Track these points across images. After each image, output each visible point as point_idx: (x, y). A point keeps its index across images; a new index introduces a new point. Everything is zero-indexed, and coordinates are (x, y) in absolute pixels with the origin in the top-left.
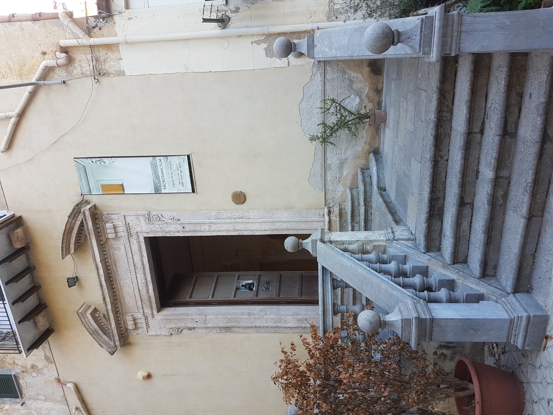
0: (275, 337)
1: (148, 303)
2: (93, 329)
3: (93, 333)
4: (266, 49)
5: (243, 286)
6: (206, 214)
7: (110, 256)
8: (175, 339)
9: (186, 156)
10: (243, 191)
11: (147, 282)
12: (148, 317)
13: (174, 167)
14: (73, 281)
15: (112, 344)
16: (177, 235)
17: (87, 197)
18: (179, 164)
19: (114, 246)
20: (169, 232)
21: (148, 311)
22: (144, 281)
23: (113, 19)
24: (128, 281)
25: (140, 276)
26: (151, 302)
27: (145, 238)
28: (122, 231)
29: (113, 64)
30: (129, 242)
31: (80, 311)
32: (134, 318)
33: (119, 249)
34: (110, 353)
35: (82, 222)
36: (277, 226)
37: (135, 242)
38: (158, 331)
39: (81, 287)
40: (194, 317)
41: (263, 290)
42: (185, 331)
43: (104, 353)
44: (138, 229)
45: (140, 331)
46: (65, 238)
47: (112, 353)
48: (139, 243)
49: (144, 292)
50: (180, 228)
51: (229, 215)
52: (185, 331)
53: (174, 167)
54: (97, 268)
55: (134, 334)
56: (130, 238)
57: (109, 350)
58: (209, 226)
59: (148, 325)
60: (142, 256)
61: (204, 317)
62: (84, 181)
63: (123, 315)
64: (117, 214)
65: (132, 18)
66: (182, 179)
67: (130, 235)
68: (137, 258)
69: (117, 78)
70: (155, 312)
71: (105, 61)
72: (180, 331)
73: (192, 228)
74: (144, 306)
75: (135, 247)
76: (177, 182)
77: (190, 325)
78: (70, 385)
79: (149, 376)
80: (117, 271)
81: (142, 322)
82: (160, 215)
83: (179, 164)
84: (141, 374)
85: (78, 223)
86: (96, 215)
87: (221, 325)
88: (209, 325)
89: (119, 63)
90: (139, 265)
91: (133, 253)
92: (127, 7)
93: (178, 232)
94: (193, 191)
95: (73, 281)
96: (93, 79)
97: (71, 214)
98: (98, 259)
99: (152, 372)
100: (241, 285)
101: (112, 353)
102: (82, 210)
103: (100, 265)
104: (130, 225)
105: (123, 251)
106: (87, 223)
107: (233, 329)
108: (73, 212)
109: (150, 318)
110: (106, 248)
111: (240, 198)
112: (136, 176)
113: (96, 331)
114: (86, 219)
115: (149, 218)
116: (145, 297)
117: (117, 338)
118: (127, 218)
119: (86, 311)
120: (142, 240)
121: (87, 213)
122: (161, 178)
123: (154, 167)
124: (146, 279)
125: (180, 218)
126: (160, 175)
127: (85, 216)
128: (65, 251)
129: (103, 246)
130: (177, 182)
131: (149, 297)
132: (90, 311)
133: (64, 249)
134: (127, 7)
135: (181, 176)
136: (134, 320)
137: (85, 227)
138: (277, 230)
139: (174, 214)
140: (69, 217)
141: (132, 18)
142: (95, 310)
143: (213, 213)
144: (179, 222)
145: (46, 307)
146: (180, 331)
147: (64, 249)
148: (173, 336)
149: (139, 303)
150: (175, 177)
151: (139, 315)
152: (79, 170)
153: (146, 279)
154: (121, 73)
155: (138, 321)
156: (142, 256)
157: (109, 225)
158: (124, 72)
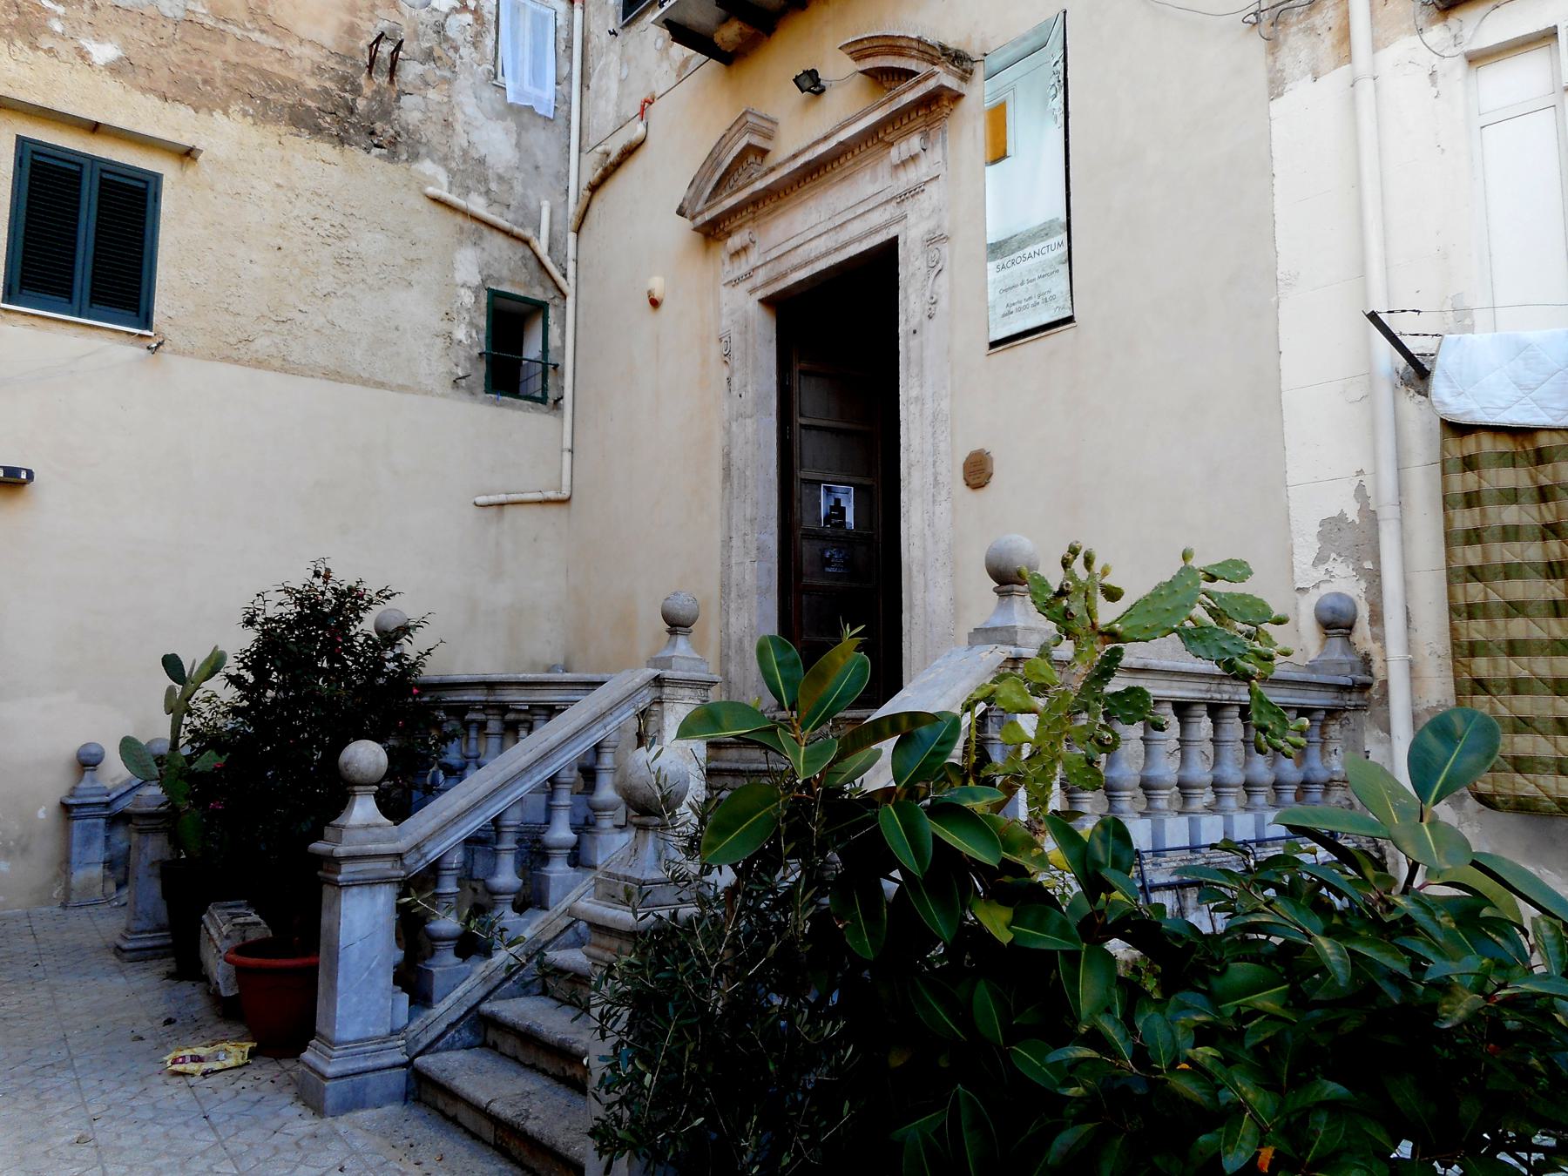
0: (714, 589)
1: (773, 274)
3: (713, 158)
4: (1342, 517)
5: (838, 501)
8: (716, 350)
9: (1068, 313)
10: (993, 479)
13: (1045, 285)
14: (811, 83)
15: (698, 208)
16: (902, 318)
17: (980, 72)
18: (1053, 298)
19: (879, 168)
20: (906, 298)
21: (761, 276)
23: (1433, 23)
24: (813, 218)
26: (776, 280)
28: (912, 175)
29: (1303, 55)
30: (887, 202)
31: (750, 118)
33: (874, 180)
34: (681, 207)
35: (914, 74)
36: (918, 579)
37: (887, 216)
39: (807, 104)
41: (823, 551)
43: (679, 192)
44: (912, 219)
45: (727, 267)
46: (880, 42)
47: (681, 212)
48: (887, 225)
49: (796, 258)
50: (913, 324)
51: (943, 447)
52: (726, 373)
53: (1045, 285)
54: (826, 138)
56: (894, 203)
57: (686, 205)
58: (917, 399)
59: (735, 282)
60: (859, 239)
62: (1012, 53)
63: (753, 219)
64: (945, 160)
65: (1434, 83)
66: (1019, 310)
67: (901, 198)
68: (856, 228)
69: (1260, 76)
70: (760, 294)
71: (1311, 30)
73: (914, 355)
75: (877, 218)
76: (1011, 297)
77: (735, 380)
78: (640, 129)
79: (655, 303)
80: (834, 185)
81: (743, 266)
83: (1053, 298)
84: (657, 285)
85: (911, 65)
86: (937, 103)
89: (1304, 74)
90: (844, 235)
92: (1476, 59)
94: (994, 345)
95: (811, 83)
96: (1253, 9)
97: (925, 43)
98: (843, 136)
99: (664, 308)
100: (839, 496)
101: (681, 212)
102: (936, 69)
103: (833, 143)
104: (921, 197)
105: (870, 189)
106: (911, 88)
109: (748, 285)
111: (977, 472)
112: (1019, 194)
113: (719, 164)
114: (918, 82)
115: (934, 240)
118: (934, 184)
119: (754, 131)
121: (931, 84)
122: (1020, 253)
123: (1044, 232)
124: (817, 258)
125: (935, 319)
126: (1028, 250)
127: (926, 78)
128: (859, 50)
129: (877, 137)
130: (1011, 297)
131: (785, 275)
132: (756, 141)
133: (859, 47)
134: (1476, 59)
135: (1026, 307)
136: (745, 249)
137: (903, 86)
138: (910, 577)
139: (943, 304)
140: (919, 40)
141: (1434, 83)
142: (764, 153)
143: (945, 405)
144: (925, 318)
147: (859, 47)
149: (775, 253)
150: (1017, 293)
151: (753, 258)
152: (1036, 31)
153: (817, 258)
154: (1276, 87)
155: (743, 258)
156: (859, 239)
157: (914, 143)
158: (1280, 95)
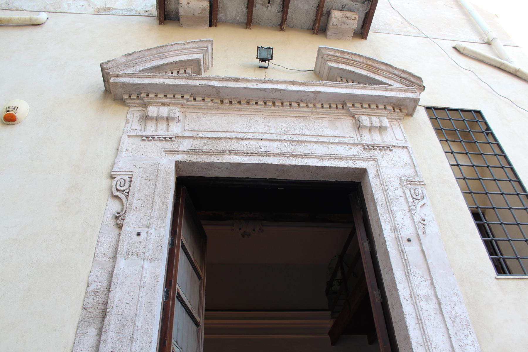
2: (167, 54)
6: (456, 295)
7: (318, 113)
11: (260, 154)
12: (170, 143)
21: (186, 145)
22: (263, 150)
25: (275, 147)
27: (363, 172)
32: (173, 119)
38: (128, 154)
40: (152, 231)
42: (115, 207)
43: (115, 52)
48: (353, 158)
52: (115, 207)
55: (129, 116)
60: (322, 157)
61: (149, 254)
63: (182, 105)
68: (319, 149)
70: (179, 157)
72: (119, 194)
74: (200, 141)
82: (425, 201)
87: (116, 294)
88: (121, 263)
90: (300, 149)
91: (330, 146)
93: (394, 229)
107: (93, 332)
108: (414, 76)
109: (167, 145)
110: (335, 111)
116: (221, 146)
117: (137, 81)
120: (359, 164)
145: (210, 26)
146: (119, 194)
147: (338, 54)
148: (108, 180)
151: (175, 129)
